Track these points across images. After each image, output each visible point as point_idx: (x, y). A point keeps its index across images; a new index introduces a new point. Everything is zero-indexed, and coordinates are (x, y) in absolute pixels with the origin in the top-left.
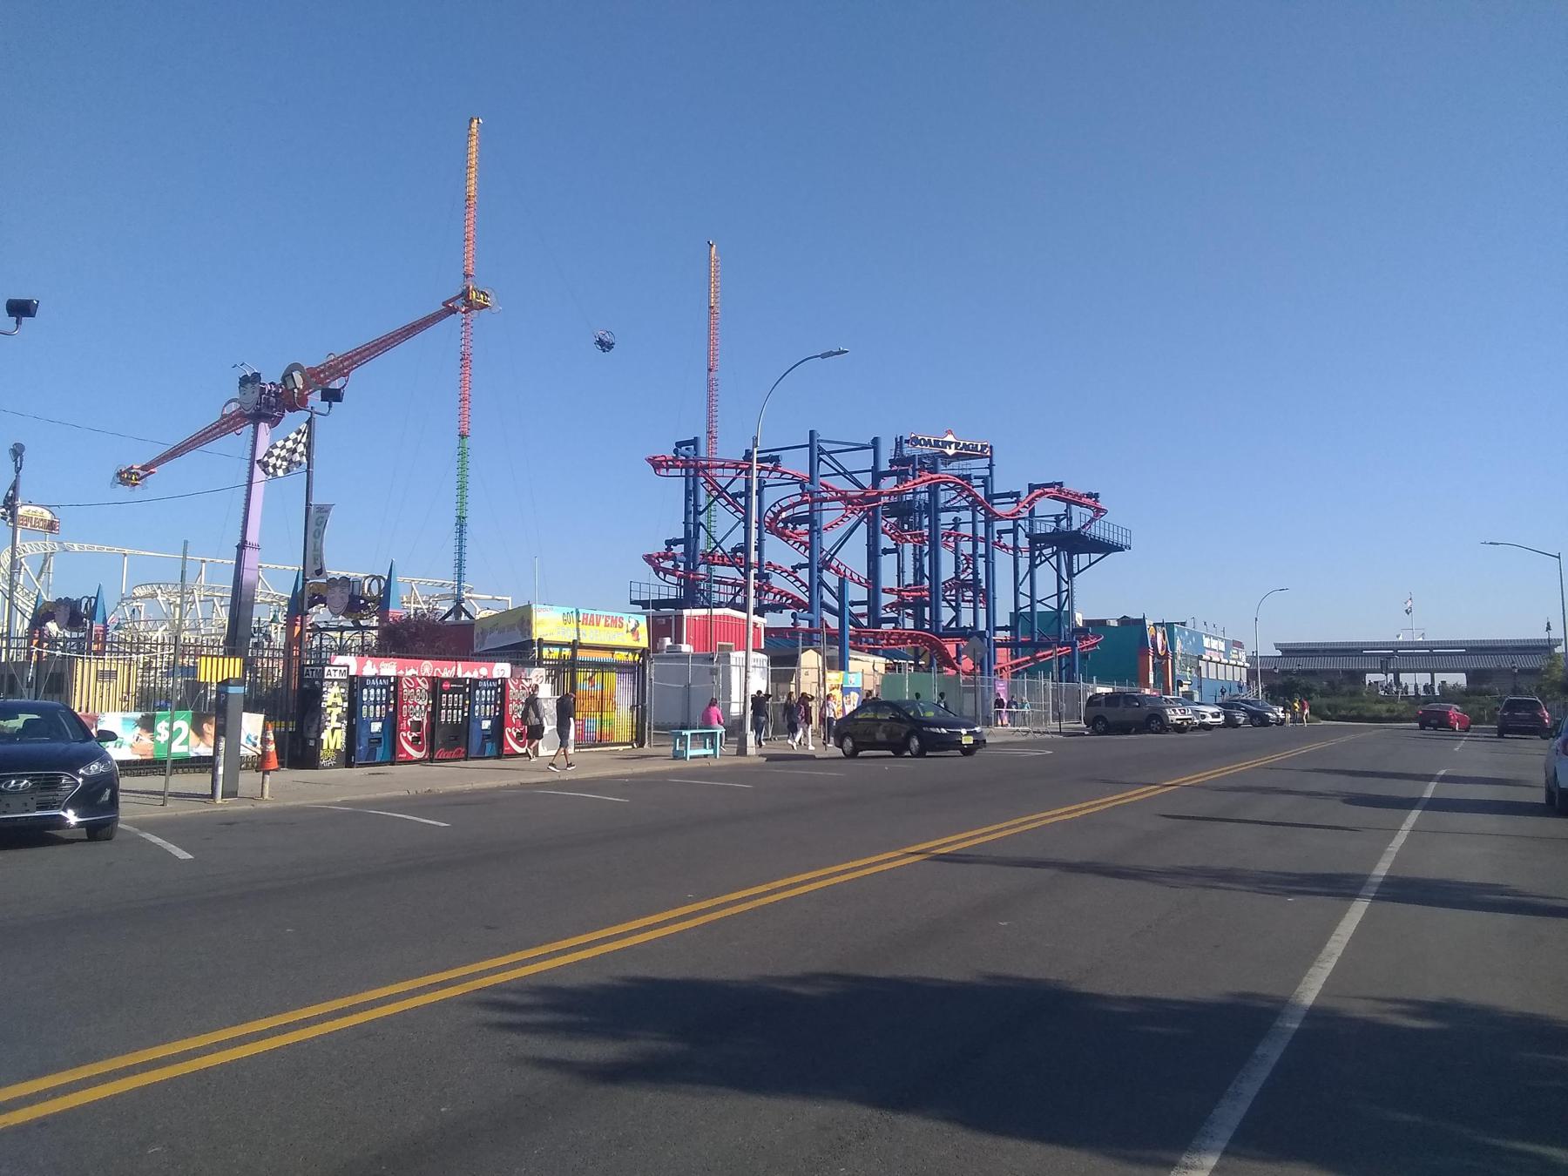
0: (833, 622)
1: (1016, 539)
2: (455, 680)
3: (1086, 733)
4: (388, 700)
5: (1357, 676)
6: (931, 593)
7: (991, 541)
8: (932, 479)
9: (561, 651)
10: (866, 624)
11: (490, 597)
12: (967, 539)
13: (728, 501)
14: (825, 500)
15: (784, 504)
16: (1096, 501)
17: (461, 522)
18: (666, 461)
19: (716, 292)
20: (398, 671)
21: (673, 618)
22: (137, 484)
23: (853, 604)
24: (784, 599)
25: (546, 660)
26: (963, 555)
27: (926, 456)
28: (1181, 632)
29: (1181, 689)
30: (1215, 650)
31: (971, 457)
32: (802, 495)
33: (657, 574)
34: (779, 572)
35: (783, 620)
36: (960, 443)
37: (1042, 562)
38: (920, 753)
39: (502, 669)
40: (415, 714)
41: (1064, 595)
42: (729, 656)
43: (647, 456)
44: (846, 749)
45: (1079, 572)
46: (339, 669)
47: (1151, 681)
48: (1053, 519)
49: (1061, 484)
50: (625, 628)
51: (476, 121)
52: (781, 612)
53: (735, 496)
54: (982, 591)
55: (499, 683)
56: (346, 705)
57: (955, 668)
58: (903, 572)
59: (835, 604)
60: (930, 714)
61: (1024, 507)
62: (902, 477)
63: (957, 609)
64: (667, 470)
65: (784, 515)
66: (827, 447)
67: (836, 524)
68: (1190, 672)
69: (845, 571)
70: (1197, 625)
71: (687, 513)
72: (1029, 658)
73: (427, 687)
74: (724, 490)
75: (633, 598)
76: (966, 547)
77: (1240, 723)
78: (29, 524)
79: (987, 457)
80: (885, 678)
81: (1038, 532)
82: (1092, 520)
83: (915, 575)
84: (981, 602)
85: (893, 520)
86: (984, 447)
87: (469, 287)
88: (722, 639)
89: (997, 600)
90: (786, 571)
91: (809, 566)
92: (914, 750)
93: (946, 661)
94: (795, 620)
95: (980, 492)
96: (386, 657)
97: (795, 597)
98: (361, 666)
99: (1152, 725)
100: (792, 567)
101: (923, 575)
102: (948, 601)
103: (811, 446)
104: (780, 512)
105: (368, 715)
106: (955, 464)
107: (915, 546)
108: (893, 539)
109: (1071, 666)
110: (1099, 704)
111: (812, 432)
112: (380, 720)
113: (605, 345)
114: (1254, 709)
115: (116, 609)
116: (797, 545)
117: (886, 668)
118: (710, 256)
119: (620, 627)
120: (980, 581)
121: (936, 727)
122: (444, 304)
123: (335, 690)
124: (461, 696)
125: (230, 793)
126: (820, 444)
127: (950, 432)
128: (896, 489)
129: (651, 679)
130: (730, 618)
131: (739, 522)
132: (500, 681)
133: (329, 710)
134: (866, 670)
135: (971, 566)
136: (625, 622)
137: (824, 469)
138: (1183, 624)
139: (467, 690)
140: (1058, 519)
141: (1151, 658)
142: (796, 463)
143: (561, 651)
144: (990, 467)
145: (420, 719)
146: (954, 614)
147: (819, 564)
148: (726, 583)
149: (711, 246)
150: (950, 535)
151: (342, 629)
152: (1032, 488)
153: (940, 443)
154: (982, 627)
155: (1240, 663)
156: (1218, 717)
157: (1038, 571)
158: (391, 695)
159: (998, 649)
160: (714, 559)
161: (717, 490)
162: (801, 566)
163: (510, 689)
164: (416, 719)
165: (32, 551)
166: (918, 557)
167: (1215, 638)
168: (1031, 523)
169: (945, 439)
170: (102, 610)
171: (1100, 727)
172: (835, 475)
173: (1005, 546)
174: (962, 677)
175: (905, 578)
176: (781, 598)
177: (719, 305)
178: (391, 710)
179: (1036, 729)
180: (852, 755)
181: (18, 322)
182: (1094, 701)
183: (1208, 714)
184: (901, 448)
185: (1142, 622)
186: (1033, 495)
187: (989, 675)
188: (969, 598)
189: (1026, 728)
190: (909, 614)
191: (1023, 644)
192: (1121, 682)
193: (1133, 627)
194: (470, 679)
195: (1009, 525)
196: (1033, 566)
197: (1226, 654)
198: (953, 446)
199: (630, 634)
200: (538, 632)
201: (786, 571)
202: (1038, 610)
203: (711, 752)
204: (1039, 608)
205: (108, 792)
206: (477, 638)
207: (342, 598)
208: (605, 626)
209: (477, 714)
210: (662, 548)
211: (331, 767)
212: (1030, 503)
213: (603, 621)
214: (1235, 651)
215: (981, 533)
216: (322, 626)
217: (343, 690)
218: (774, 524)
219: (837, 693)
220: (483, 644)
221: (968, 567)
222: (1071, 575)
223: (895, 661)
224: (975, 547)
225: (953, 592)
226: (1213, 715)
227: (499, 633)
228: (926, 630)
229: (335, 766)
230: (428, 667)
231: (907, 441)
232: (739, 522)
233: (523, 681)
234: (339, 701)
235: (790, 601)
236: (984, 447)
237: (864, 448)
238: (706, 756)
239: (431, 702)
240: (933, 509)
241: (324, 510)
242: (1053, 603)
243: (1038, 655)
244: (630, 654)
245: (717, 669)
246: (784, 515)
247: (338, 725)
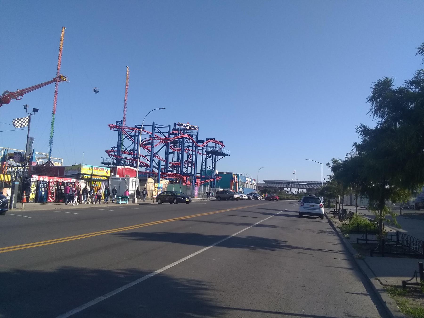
0: (156, 171)
1: (203, 151)
2: (62, 182)
3: (216, 200)
4: (46, 187)
5: (282, 189)
6: (181, 165)
7: (197, 152)
8: (183, 136)
9: (88, 176)
10: (164, 171)
11: (57, 158)
12: (191, 151)
13: (129, 137)
14: (156, 139)
15: (145, 140)
16: (223, 143)
17: (51, 138)
18: (113, 126)
19: (128, 80)
20: (48, 179)
21: (114, 168)
23: (162, 166)
24: (142, 163)
25: (84, 178)
26: (189, 154)
27: (182, 129)
28: (241, 176)
29: (240, 190)
30: (248, 181)
33: (109, 156)
34: (142, 156)
35: (143, 169)
37: (208, 158)
38: (177, 203)
39: (73, 180)
40: (53, 190)
41: (214, 166)
42: (129, 179)
43: (109, 124)
44: (159, 202)
45: (217, 161)
46: (35, 178)
47: (233, 188)
48: (212, 147)
49: (214, 139)
50: (104, 171)
51: (64, 28)
52: (142, 167)
53: (131, 136)
54: (193, 164)
55: (73, 184)
56: (36, 187)
57: (186, 183)
58: (174, 158)
59: (157, 166)
60: (179, 194)
61: (205, 144)
62: (175, 135)
63: (187, 168)
64: (114, 129)
65: (145, 143)
66: (157, 126)
67: (158, 145)
68: (242, 186)
70: (245, 175)
71: (118, 140)
72: (204, 181)
73: (56, 184)
74: (129, 135)
75: (102, 162)
76: (190, 153)
77: (251, 199)
79: (197, 130)
80: (168, 185)
81: (208, 150)
82: (221, 148)
83: (177, 159)
84: (193, 167)
85: (172, 145)
86: (196, 127)
87: (61, 75)
89: (197, 166)
90: (144, 157)
91: (151, 155)
92: (175, 202)
93: (184, 181)
94: (146, 170)
95: (195, 140)
96: (45, 176)
97: (146, 164)
98: (39, 178)
100: (145, 155)
101: (179, 159)
102: (185, 166)
103: (153, 125)
104: (144, 142)
106: (189, 131)
107: (177, 152)
108: (172, 150)
109: (214, 184)
110: (219, 193)
111: (153, 122)
113: (96, 92)
114: (255, 195)
116: (147, 150)
117: (169, 183)
118: (127, 70)
119: (103, 171)
120: (193, 161)
124: (64, 186)
125: (14, 208)
126: (155, 125)
127: (188, 123)
128: (174, 138)
129: (110, 184)
131: (132, 143)
132: (48, 181)
133: (32, 189)
134: (164, 183)
135: (191, 157)
136: (105, 169)
137: (156, 131)
138: (241, 174)
139: (65, 185)
141: (233, 182)
142: (149, 129)
143: (88, 176)
144: (198, 133)
145: (54, 192)
146: (186, 169)
147: (153, 155)
148: (128, 159)
149: (127, 67)
150: (187, 150)
151: (18, 166)
152: (207, 139)
153: (185, 126)
154: (193, 173)
155: (254, 184)
156: (246, 197)
158: (47, 185)
159: (197, 179)
160: (124, 153)
161: (127, 135)
162: (148, 155)
163: (76, 185)
164: (53, 192)
166: (178, 154)
167: (249, 178)
168: (207, 148)
169: (187, 125)
171: (219, 199)
172: (158, 133)
173: (200, 153)
174: (187, 186)
175: (175, 160)
176: (142, 164)
177: (128, 83)
178: (47, 189)
179: (204, 199)
180: (160, 203)
182: (218, 192)
183: (244, 196)
184: (176, 126)
185: (232, 173)
186: (207, 141)
187: (194, 185)
188: (190, 166)
189: (201, 199)
190: (175, 169)
191: (203, 178)
192: (225, 188)
193: (230, 174)
194: (66, 182)
195: (201, 148)
196: (206, 159)
197: (251, 182)
198: (189, 127)
199: (106, 173)
201: (144, 157)
202: (207, 169)
203: (126, 202)
204: (207, 169)
205: (7, 204)
206: (65, 172)
207: (19, 158)
210: (111, 149)
211: (31, 203)
212: (207, 143)
213: (99, 169)
214: (254, 182)
215: (194, 149)
216: (12, 165)
217: (35, 184)
218: (142, 145)
219: (156, 189)
220: (67, 173)
221: (191, 158)
222: (215, 161)
223: (171, 181)
224: (193, 153)
225: (187, 164)
226: (245, 197)
227: (72, 171)
228: (179, 174)
229: (33, 203)
230: (55, 179)
231: (177, 125)
232: (132, 143)
233: (79, 183)
234: (34, 186)
235: (145, 165)
236: (196, 127)
238: (124, 203)
239: (56, 188)
240: (183, 143)
241: (32, 139)
242: (211, 168)
243: (206, 181)
245: (127, 182)
246: (145, 143)
247: (34, 192)
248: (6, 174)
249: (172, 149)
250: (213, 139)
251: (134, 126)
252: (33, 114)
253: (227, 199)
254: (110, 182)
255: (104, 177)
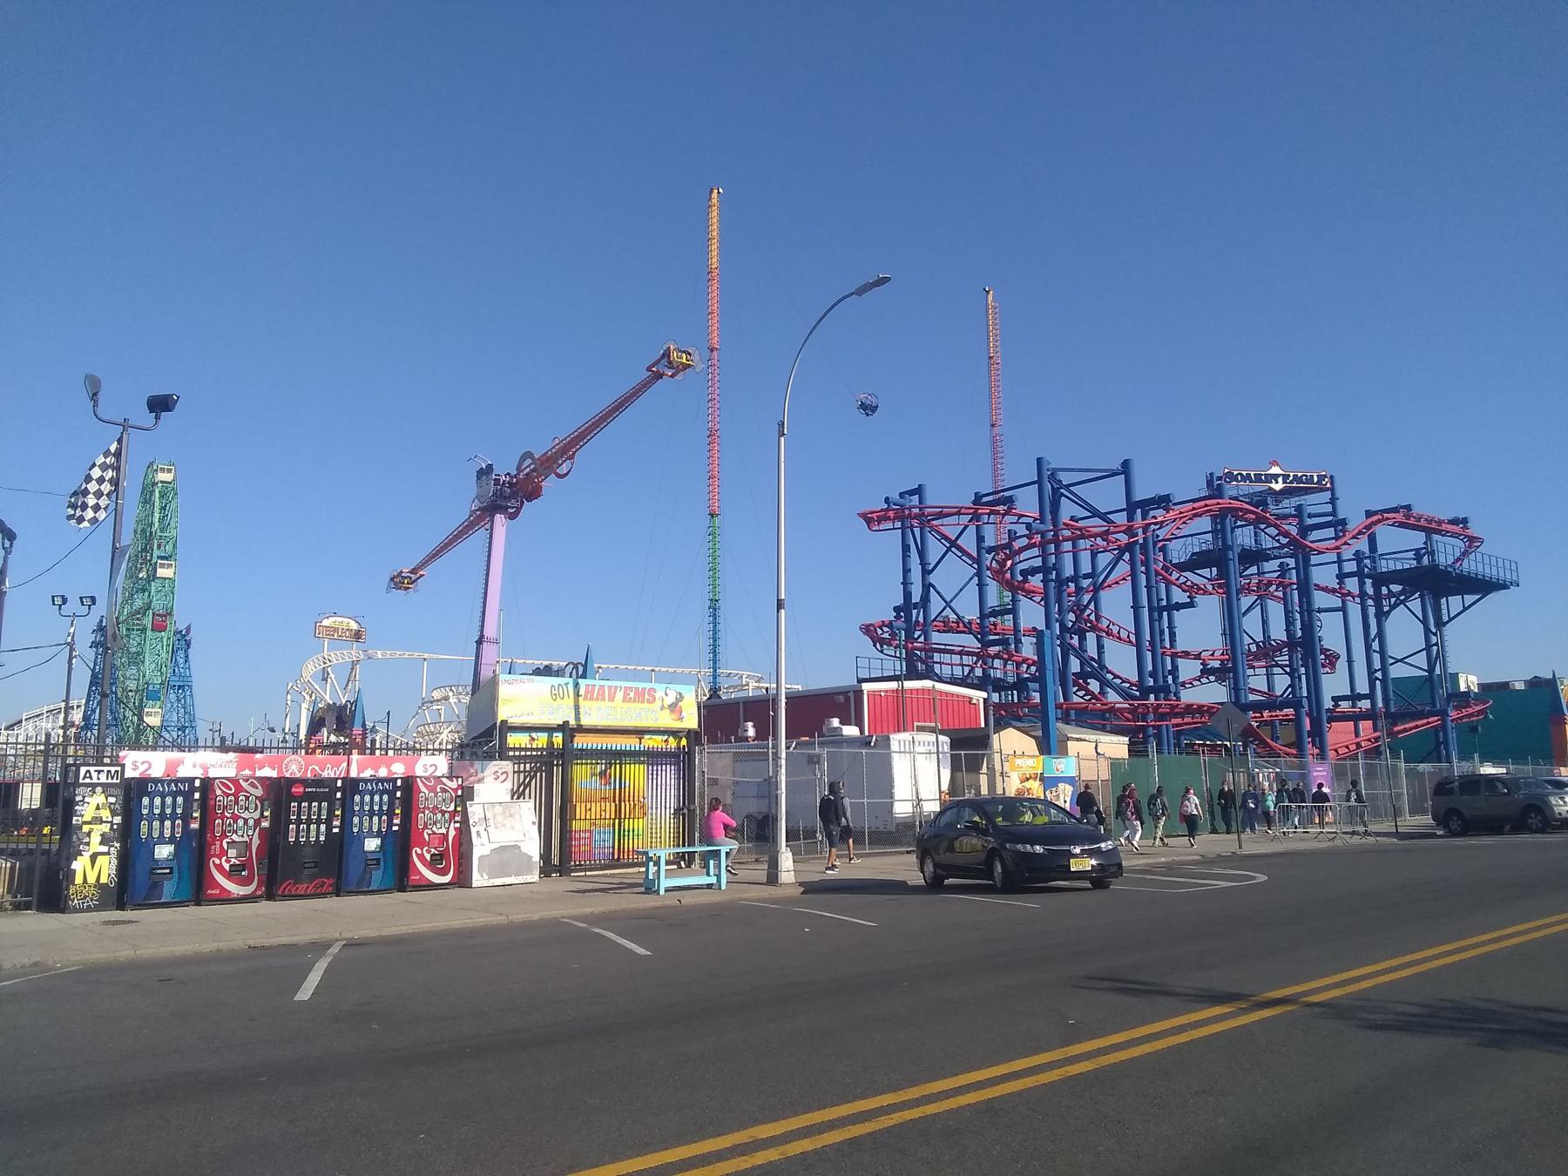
9: (550, 737)
21: (851, 695)
22: (409, 588)
31: (1307, 491)
32: (1029, 537)
33: (875, 646)
36: (1289, 475)
37: (1393, 607)
41: (1434, 652)
42: (889, 739)
43: (863, 510)
45: (1450, 620)
48: (1411, 555)
49: (1408, 507)
50: (658, 703)
56: (118, 820)
69: (1119, 632)
73: (259, 792)
78: (336, 635)
79: (1328, 489)
82: (1465, 554)
87: (669, 348)
88: (921, 717)
99: (1529, 821)
105: (360, 829)
111: (1039, 460)
112: (172, 840)
115: (417, 713)
119: (648, 701)
121: (1024, 843)
122: (649, 369)
123: (99, 798)
124: (325, 804)
127: (1275, 463)
130: (920, 692)
133: (86, 828)
140: (1418, 555)
142: (1027, 503)
144: (1333, 501)
145: (443, 831)
148: (952, 652)
149: (988, 292)
153: (1263, 477)
157: (1389, 625)
165: (337, 660)
169: (1269, 472)
170: (361, 716)
178: (195, 826)
181: (157, 418)
192: (1519, 758)
198: (1280, 479)
199: (667, 711)
200: (504, 713)
208: (624, 700)
209: (355, 830)
211: (89, 910)
213: (620, 695)
217: (112, 800)
222: (1440, 624)
229: (97, 909)
234: (105, 814)
236: (1321, 478)
237: (1114, 474)
244: (671, 739)
245: (819, 756)
248: (630, 764)
249: (1180, 587)
250: (1402, 507)
251: (967, 501)
252: (146, 426)
253: (1508, 827)
254: (700, 760)
255: (665, 737)
